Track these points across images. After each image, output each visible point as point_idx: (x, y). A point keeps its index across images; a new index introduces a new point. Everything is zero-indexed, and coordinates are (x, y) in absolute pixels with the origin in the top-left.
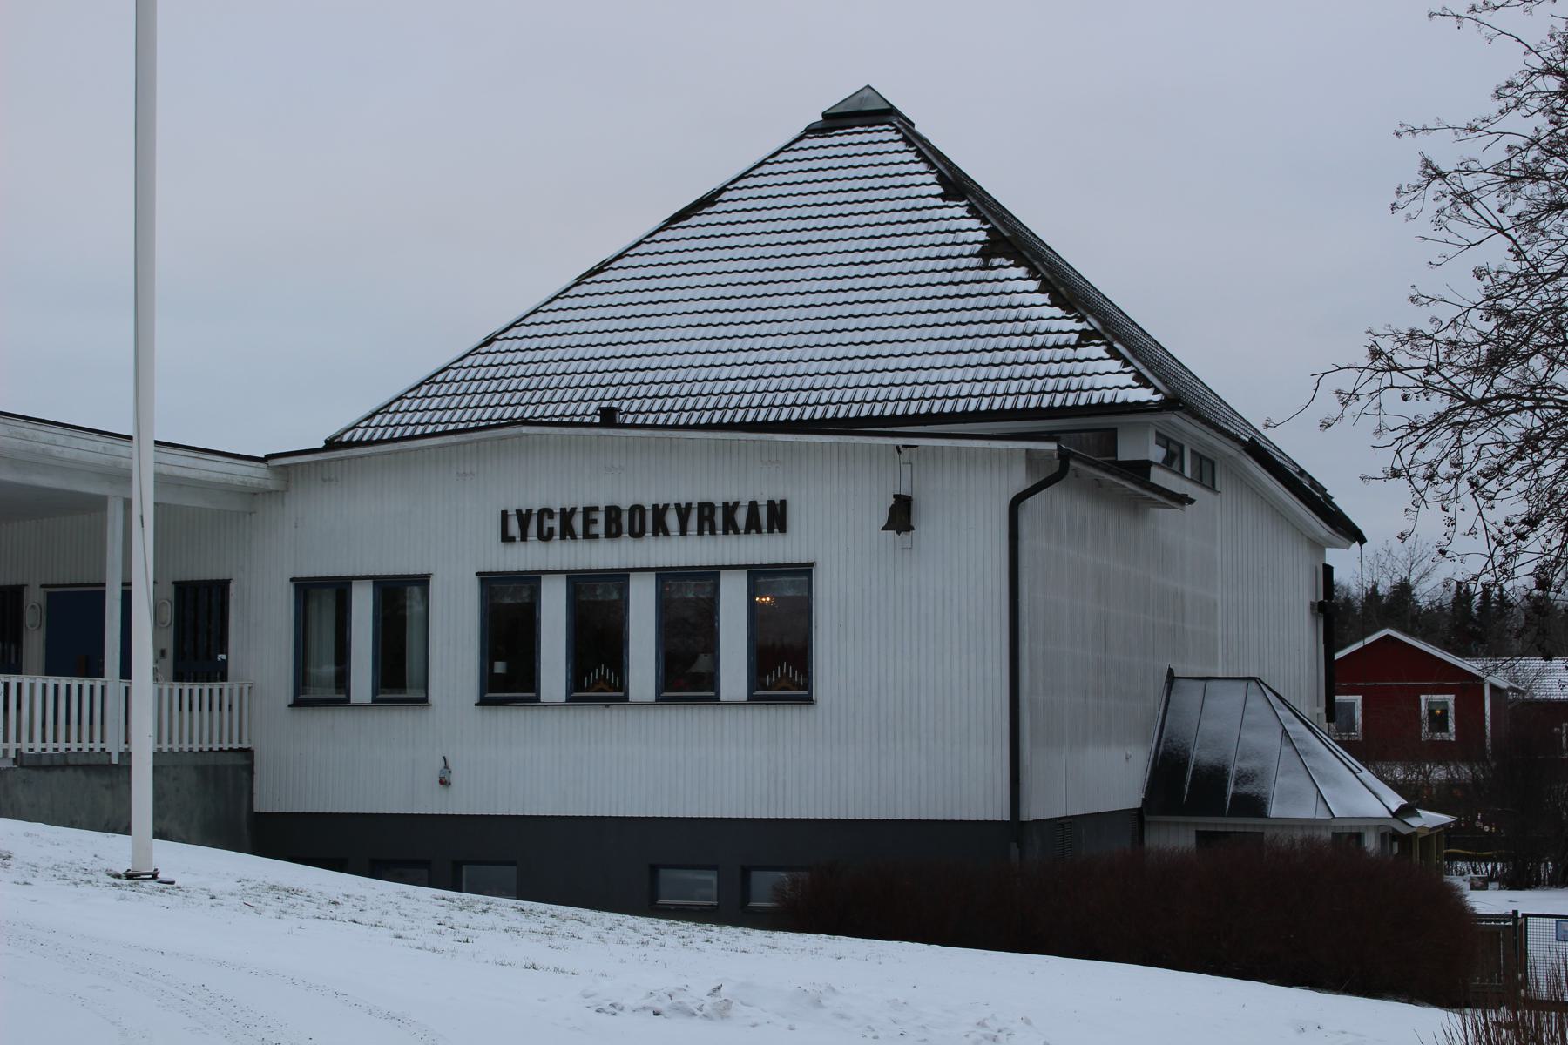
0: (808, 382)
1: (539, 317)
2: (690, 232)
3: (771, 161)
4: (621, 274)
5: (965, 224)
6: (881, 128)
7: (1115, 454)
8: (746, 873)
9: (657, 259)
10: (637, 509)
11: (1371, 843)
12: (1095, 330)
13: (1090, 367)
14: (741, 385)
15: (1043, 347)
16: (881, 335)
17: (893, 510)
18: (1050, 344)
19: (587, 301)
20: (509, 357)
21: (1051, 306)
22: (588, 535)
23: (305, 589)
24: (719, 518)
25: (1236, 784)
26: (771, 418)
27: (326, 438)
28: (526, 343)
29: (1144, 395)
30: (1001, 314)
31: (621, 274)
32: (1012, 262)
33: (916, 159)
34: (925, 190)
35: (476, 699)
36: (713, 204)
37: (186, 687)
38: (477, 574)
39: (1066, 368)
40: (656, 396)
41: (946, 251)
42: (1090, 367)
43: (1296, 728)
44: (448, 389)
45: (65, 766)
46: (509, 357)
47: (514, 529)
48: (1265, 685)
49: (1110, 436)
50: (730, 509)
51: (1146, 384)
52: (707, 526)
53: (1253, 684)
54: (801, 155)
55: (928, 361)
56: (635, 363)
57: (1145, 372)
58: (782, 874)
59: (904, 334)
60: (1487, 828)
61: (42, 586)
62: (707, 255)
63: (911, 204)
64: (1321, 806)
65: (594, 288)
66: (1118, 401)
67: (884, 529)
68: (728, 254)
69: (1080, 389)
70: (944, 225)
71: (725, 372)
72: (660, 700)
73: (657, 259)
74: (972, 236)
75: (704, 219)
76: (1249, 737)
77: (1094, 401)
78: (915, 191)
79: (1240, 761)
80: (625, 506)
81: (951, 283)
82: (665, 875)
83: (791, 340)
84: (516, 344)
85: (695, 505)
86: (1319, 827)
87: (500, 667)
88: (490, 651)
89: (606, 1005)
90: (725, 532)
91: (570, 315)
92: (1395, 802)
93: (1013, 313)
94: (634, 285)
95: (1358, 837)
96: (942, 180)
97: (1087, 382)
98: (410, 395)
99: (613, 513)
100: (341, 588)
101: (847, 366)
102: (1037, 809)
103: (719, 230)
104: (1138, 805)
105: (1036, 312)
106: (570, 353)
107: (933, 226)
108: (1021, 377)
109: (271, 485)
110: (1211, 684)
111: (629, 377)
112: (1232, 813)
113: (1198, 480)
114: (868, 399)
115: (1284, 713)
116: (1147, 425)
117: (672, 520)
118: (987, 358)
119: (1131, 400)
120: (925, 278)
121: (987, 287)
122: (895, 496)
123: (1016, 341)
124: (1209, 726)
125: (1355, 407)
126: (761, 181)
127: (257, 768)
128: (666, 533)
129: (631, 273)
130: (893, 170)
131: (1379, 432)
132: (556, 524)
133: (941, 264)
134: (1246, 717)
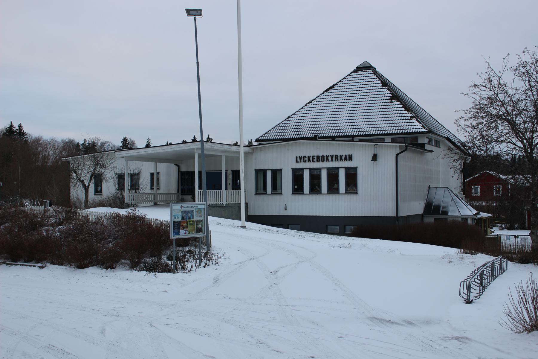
0: (355, 127)
1: (298, 113)
2: (329, 94)
3: (345, 78)
4: (315, 103)
5: (387, 92)
6: (369, 70)
7: (418, 142)
8: (345, 226)
9: (322, 100)
10: (323, 156)
11: (470, 221)
12: (414, 116)
13: (413, 124)
14: (341, 128)
15: (403, 120)
16: (370, 117)
17: (373, 157)
18: (404, 119)
19: (308, 109)
20: (293, 121)
21: (405, 111)
22: (313, 161)
23: (257, 171)
24: (339, 158)
25: (442, 209)
26: (347, 135)
27: (256, 139)
28: (296, 118)
29: (424, 130)
30: (394, 112)
31: (315, 103)
32: (397, 101)
33: (376, 78)
34: (378, 85)
35: (292, 193)
36: (334, 88)
37: (234, 191)
38: (292, 169)
39: (408, 124)
40: (323, 130)
41: (383, 98)
42: (413, 124)
43: (455, 197)
44: (280, 128)
45: (217, 207)
46: (293, 121)
47: (299, 160)
48: (450, 190)
49: (416, 139)
50: (341, 156)
51: (424, 128)
52: (337, 159)
53: (446, 188)
54: (352, 77)
55: (379, 123)
56: (319, 123)
57: (424, 125)
58: (352, 227)
59: (374, 117)
60: (503, 217)
61: (206, 171)
62: (333, 99)
63: (375, 88)
64: (459, 213)
65: (309, 106)
66: (418, 131)
67: (371, 160)
68: (337, 99)
69: (411, 129)
70: (382, 93)
71: (338, 125)
72: (328, 193)
73: (322, 100)
74: (388, 95)
75: (332, 91)
76: (445, 199)
77: (413, 131)
78: (376, 85)
79: (443, 204)
80: (320, 155)
81: (384, 105)
82: (329, 227)
83: (351, 118)
84: (294, 119)
85: (334, 156)
86: (459, 217)
87: (296, 187)
88: (294, 184)
89: (332, 246)
90: (340, 161)
91: (305, 112)
92: (475, 212)
93: (397, 112)
94: (318, 106)
95: (467, 219)
96: (382, 82)
97: (412, 127)
98: (272, 130)
99: (318, 157)
100: (264, 172)
101: (363, 123)
102: (401, 214)
103: (335, 93)
104: (422, 213)
105: (402, 112)
106: (305, 121)
107: (380, 93)
108: (399, 126)
109: (251, 152)
110: (437, 188)
111: (318, 126)
112: (441, 215)
113: (436, 146)
114: (367, 131)
115: (452, 194)
116: (424, 136)
117: (330, 158)
118: (392, 122)
119: (421, 131)
120: (379, 104)
121: (392, 106)
122: (373, 154)
123: (397, 118)
124: (437, 197)
125: (447, 156)
126: (344, 82)
127: (248, 206)
128: (329, 161)
129: (317, 103)
130: (372, 80)
131: (450, 160)
132: (307, 159)
133: (382, 101)
134: (444, 195)
